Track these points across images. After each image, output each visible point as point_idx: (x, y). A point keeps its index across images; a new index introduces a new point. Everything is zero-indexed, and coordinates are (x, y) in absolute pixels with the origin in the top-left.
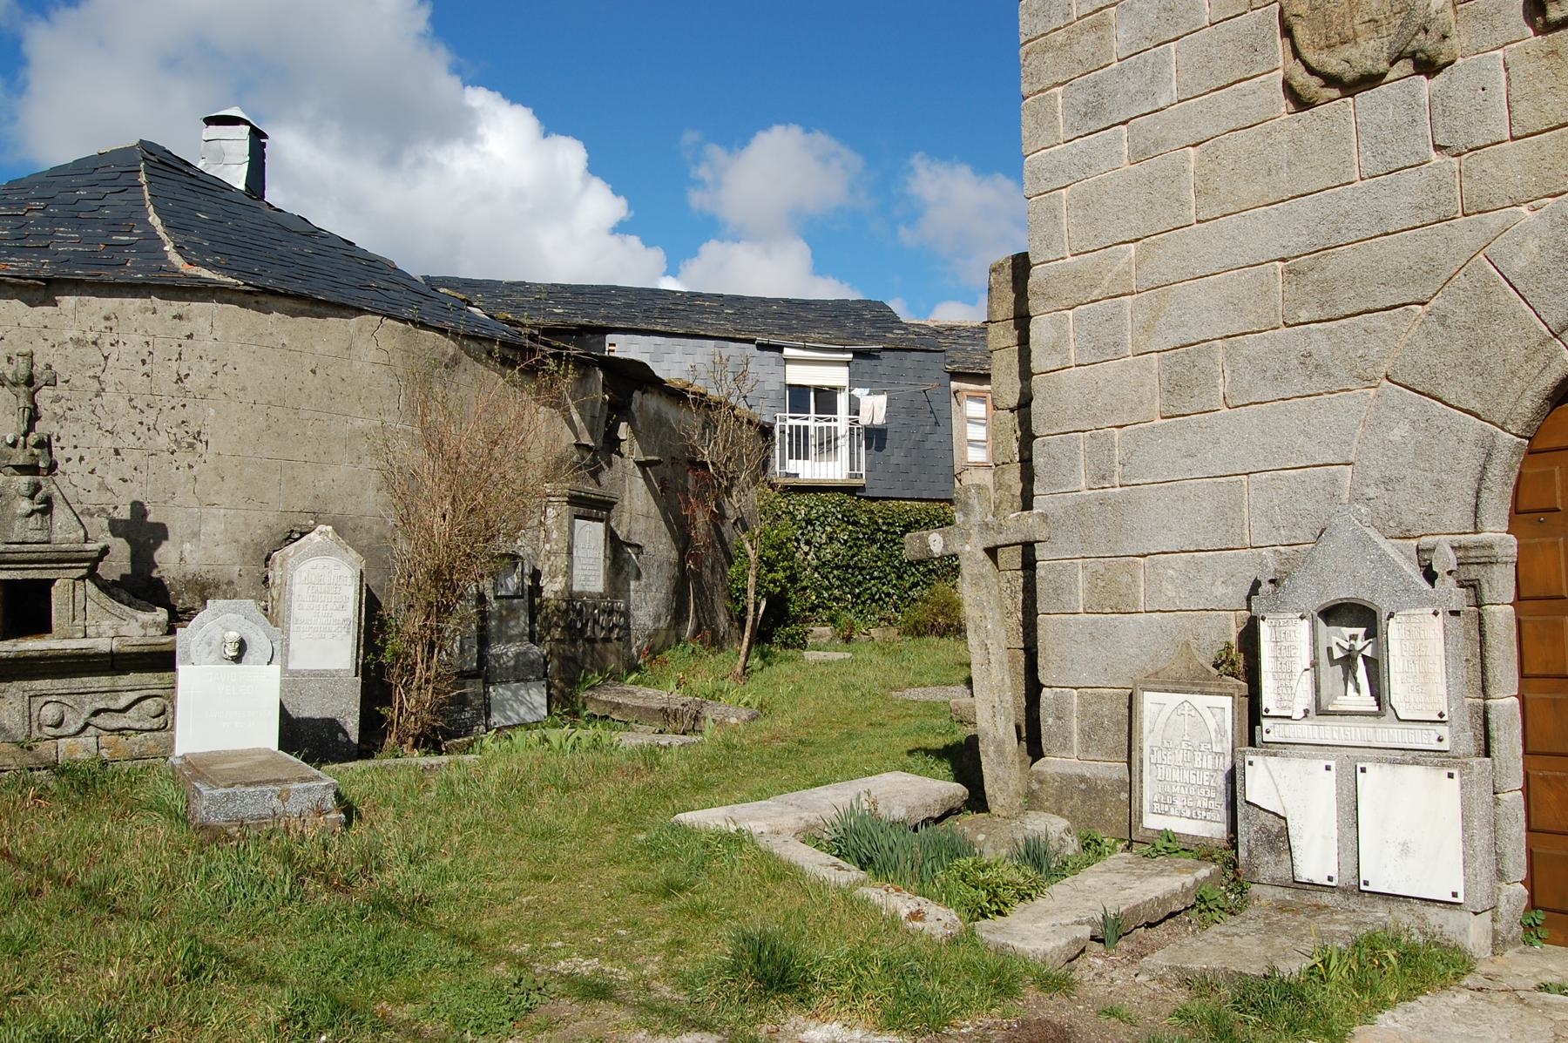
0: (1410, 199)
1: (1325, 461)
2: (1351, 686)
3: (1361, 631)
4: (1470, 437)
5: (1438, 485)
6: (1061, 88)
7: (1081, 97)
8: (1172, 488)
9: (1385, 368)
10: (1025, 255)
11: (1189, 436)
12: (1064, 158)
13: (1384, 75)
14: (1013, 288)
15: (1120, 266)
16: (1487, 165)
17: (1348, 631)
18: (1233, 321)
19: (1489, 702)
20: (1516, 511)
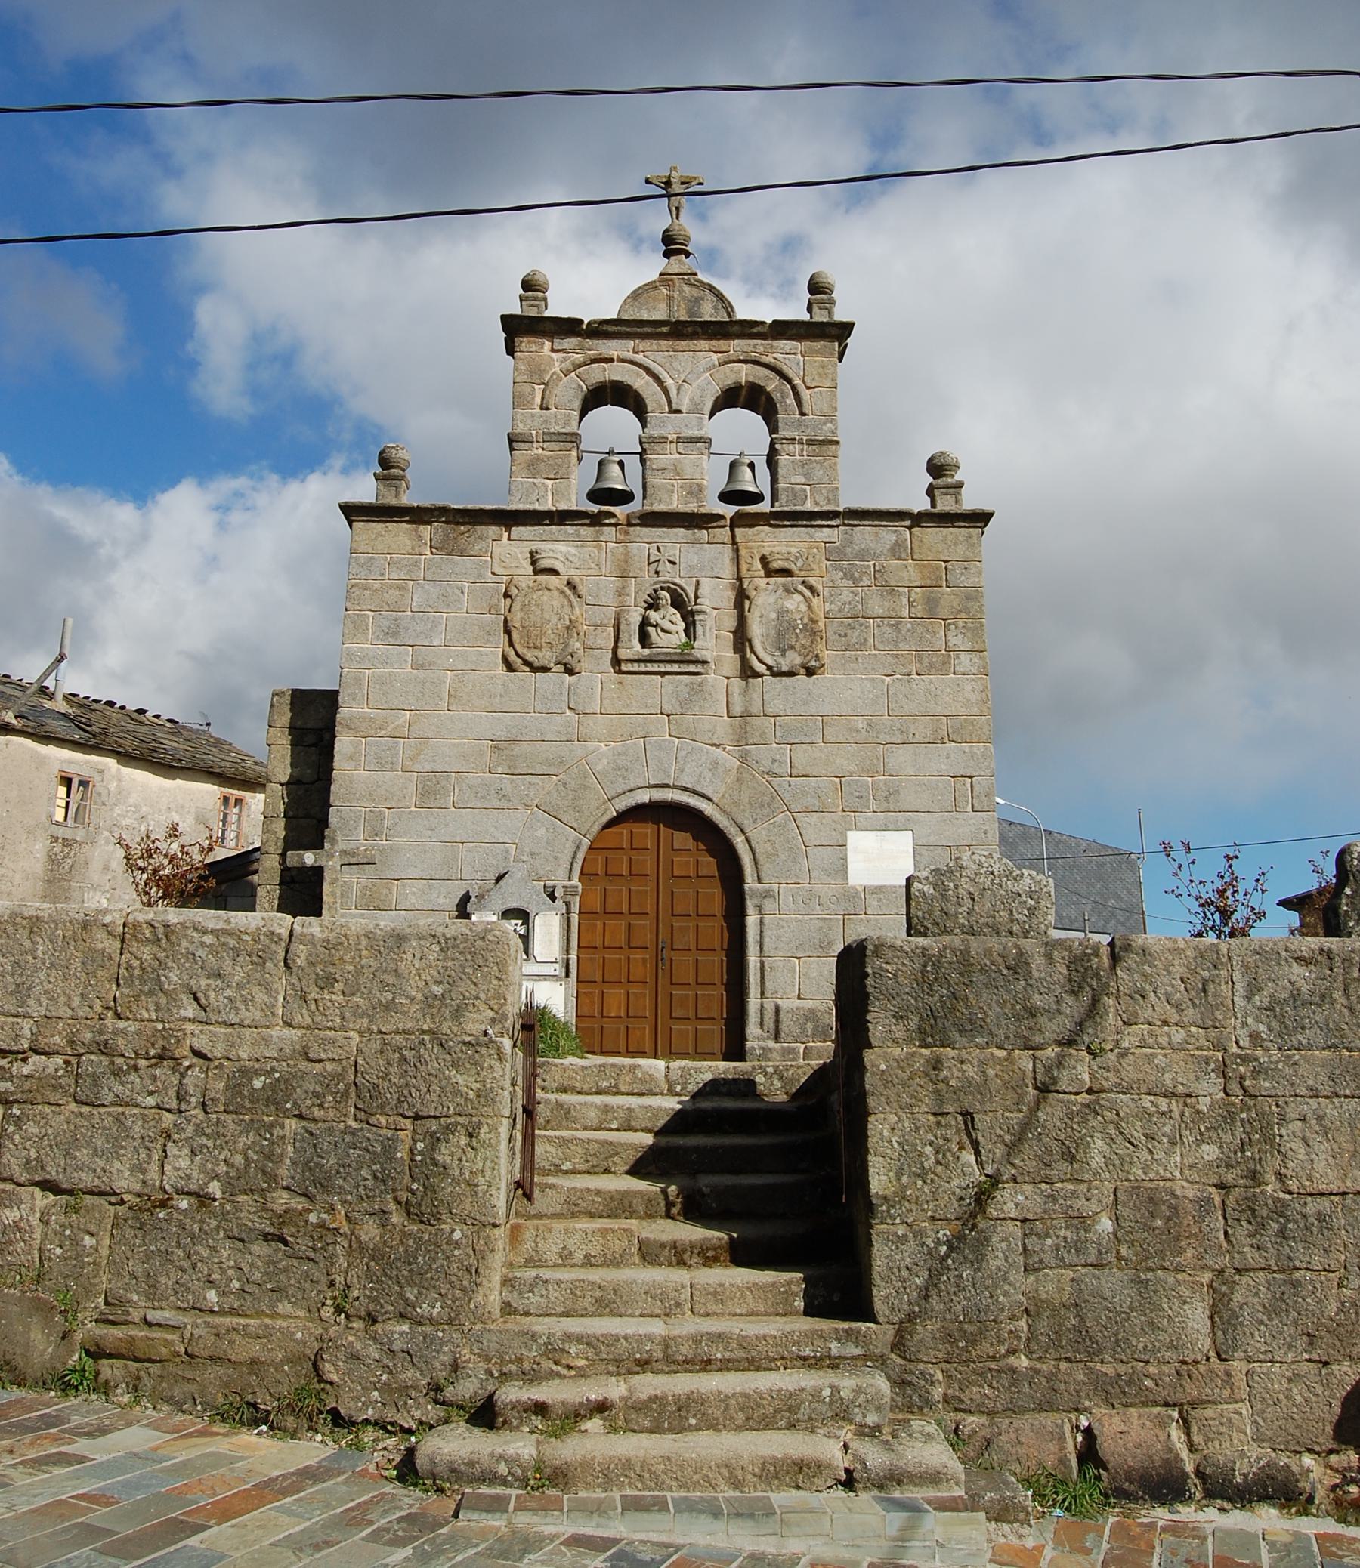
3: (520, 922)
4: (571, 839)
5: (556, 858)
6: (373, 613)
7: (386, 623)
9: (535, 803)
10: (329, 700)
11: (432, 819)
15: (400, 722)
16: (591, 722)
17: (514, 922)
20: (582, 874)
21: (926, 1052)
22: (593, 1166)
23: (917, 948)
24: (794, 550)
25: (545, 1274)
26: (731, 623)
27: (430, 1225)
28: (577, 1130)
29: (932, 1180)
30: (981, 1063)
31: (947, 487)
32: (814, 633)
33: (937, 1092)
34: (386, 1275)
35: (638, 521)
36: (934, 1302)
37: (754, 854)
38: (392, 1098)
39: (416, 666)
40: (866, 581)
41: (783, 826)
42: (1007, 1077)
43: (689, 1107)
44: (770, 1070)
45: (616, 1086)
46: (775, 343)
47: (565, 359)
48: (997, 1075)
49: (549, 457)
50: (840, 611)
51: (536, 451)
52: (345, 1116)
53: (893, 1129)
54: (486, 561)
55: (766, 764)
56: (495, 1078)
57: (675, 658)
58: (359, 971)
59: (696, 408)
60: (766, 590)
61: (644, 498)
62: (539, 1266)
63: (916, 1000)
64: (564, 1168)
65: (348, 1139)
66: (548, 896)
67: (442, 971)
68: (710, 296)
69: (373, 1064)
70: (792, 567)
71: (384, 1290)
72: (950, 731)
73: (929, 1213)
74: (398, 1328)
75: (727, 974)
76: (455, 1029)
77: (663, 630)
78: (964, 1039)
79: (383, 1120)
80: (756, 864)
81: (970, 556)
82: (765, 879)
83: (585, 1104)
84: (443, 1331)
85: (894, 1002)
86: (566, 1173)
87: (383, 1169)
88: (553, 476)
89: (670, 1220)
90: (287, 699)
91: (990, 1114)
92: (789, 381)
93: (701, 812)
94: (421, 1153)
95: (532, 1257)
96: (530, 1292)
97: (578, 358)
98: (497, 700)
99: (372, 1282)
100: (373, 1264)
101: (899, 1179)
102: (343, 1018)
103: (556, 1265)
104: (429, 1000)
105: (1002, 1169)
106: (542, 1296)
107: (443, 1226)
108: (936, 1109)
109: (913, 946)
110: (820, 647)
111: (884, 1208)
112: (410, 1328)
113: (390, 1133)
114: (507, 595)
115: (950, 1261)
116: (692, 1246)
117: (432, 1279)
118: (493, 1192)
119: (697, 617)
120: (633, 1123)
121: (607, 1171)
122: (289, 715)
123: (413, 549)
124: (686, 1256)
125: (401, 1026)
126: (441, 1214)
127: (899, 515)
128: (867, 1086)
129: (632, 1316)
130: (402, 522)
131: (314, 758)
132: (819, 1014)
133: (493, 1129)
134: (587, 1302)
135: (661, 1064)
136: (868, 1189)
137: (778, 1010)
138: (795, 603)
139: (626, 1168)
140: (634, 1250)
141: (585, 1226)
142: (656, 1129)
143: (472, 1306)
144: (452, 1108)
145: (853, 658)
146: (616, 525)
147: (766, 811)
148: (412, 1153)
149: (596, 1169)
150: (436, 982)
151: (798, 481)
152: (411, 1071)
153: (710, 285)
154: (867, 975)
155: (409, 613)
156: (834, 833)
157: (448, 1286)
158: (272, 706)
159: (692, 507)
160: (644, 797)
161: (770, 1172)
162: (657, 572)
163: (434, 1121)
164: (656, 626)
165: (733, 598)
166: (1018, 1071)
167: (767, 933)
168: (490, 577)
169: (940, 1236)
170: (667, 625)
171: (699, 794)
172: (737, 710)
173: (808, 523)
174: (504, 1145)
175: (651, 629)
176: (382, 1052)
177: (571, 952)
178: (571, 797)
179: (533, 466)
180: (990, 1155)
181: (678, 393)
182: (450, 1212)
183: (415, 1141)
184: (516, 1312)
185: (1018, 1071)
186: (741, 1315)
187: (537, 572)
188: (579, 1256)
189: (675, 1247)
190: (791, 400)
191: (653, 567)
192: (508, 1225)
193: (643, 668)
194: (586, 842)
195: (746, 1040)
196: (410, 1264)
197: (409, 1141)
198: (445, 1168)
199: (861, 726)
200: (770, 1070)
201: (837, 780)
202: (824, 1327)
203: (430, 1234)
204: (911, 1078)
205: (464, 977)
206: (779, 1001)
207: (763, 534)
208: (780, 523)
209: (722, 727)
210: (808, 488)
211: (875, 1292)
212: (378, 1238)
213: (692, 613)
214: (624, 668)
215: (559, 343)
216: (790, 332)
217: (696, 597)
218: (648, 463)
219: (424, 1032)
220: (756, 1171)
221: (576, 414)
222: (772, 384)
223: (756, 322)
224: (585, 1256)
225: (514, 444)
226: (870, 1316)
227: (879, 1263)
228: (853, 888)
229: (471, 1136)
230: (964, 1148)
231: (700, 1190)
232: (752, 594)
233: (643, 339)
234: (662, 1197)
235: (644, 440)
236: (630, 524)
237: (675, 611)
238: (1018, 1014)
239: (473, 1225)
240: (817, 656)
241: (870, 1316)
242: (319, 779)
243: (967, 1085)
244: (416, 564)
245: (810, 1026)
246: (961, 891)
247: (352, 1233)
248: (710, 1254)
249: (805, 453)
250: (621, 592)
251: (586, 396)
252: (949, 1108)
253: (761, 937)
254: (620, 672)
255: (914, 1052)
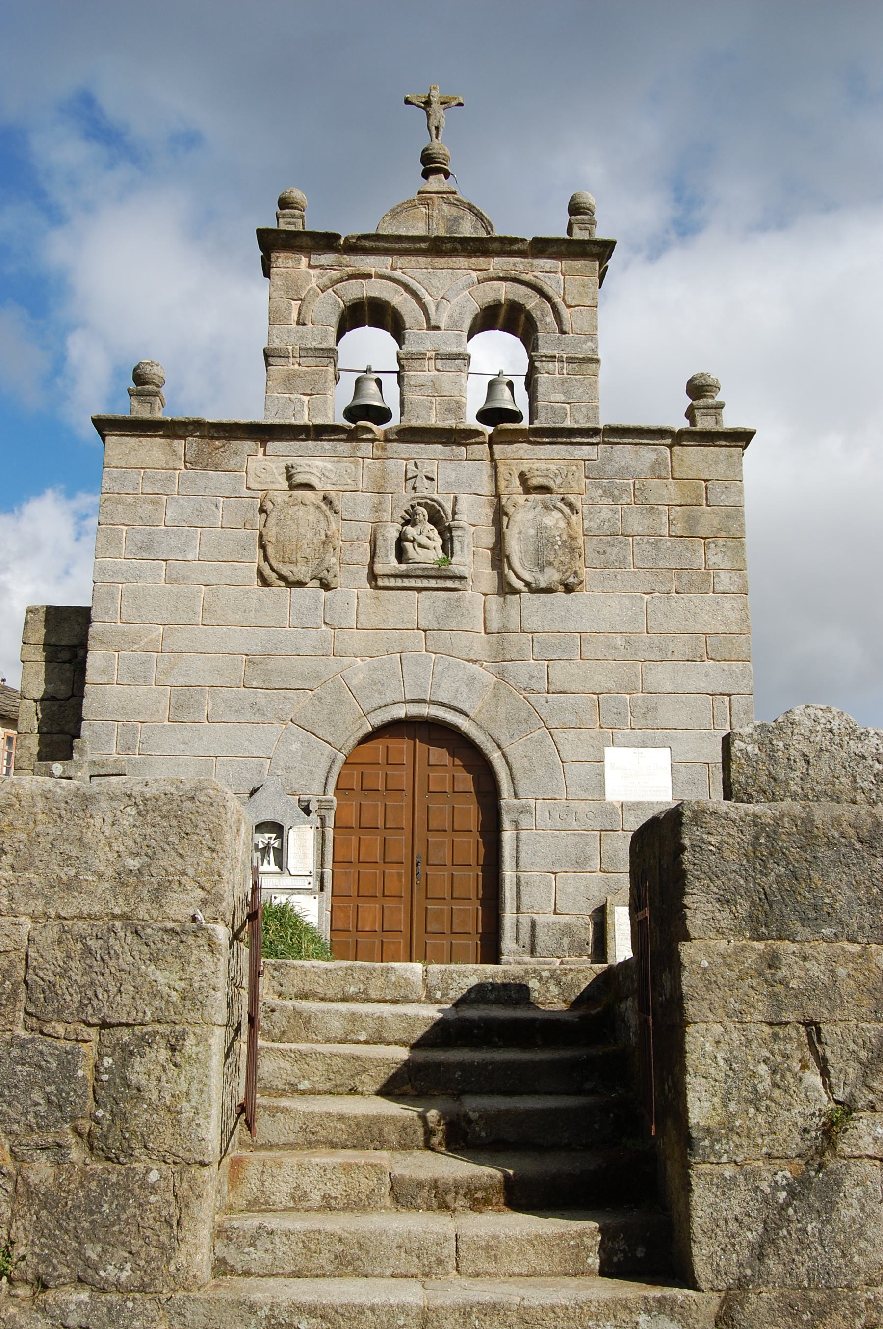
0: (311, 642)
1: (258, 755)
2: (266, 862)
3: (274, 835)
4: (326, 753)
5: (311, 772)
6: (126, 528)
7: (139, 537)
8: (172, 759)
9: (290, 717)
11: (185, 733)
12: (124, 567)
13: (307, 584)
14: (45, 626)
15: (154, 636)
16: (346, 637)
17: (267, 835)
18: (217, 679)
19: (324, 870)
20: (337, 789)
21: (760, 945)
22: (336, 1086)
23: (747, 815)
24: (553, 468)
25: (272, 1222)
26: (489, 539)
27: (119, 1163)
28: (318, 1042)
29: (768, 1107)
30: (829, 960)
31: (708, 408)
32: (573, 550)
33: (773, 996)
34: (61, 1227)
35: (395, 437)
36: (771, 1263)
37: (510, 770)
38: (73, 1000)
39: (170, 580)
40: (626, 499)
41: (540, 742)
42: (862, 978)
43: (452, 1016)
44: (546, 974)
45: (365, 991)
46: (536, 262)
47: (322, 275)
48: (849, 975)
49: (305, 373)
50: (599, 528)
51: (292, 367)
52: (11, 1023)
53: (718, 1042)
54: (241, 476)
55: (524, 680)
56: (205, 975)
57: (433, 573)
58: (34, 839)
59: (455, 325)
60: (525, 506)
61: (402, 414)
62: (265, 1211)
63: (746, 880)
64: (301, 1087)
65: (15, 1052)
66: (303, 809)
67: (139, 840)
68: (469, 216)
69: (48, 957)
70: (551, 484)
71: (57, 1247)
72: (709, 649)
73: (765, 1150)
74: (74, 1297)
75: (483, 890)
76: (155, 913)
77: (420, 546)
78: (807, 930)
79: (60, 1029)
80: (513, 779)
81: (731, 475)
82: (521, 794)
83: (328, 1011)
84: (134, 1300)
85: (719, 882)
86: (303, 1093)
87: (60, 1091)
88: (309, 392)
89: (430, 1152)
90: (42, 616)
91: (842, 1024)
92: (549, 299)
93: (458, 728)
94: (108, 1070)
95: (256, 1199)
96: (251, 1245)
97: (335, 274)
98: (252, 614)
99: (42, 1235)
100: (44, 1213)
101: (725, 1106)
102: (12, 899)
103: (287, 1209)
104: (122, 878)
105: (857, 1093)
106: (267, 1251)
107: (136, 1165)
108: (773, 1017)
109: (742, 813)
110: (579, 564)
111: (707, 1143)
112: (90, 1297)
113: (69, 1045)
114: (262, 510)
115: (791, 1211)
116: (457, 1185)
117: (121, 1232)
118: (201, 1121)
119: (454, 533)
120: (385, 1035)
121: (353, 1091)
122: (44, 631)
123: (167, 463)
124: (449, 1198)
125: (86, 910)
126: (133, 1149)
127: (661, 433)
128: (684, 987)
129: (381, 1276)
130: (156, 436)
131: (68, 674)
132: (575, 929)
133: (202, 1040)
134: (324, 1259)
135: (418, 967)
136: (686, 1120)
137: (533, 925)
138: (554, 520)
139: (377, 1087)
140: (385, 1190)
141: (324, 1160)
142: (412, 1042)
143: (172, 1268)
144: (149, 1013)
145: (612, 575)
146: (373, 441)
147: (523, 726)
148: (98, 1071)
149: (340, 1089)
150: (131, 853)
151: (558, 399)
152: (97, 965)
153: (469, 204)
154: (683, 849)
155: (163, 528)
156: (591, 749)
157: (141, 1242)
158: (26, 623)
159: (449, 423)
160: (400, 712)
161: (550, 1093)
162: (414, 488)
163: (125, 1030)
164: (412, 541)
165: (491, 515)
166: (875, 970)
167: (523, 848)
168: (245, 492)
169: (778, 1178)
170: (424, 540)
171: (456, 709)
172: (495, 626)
173: (568, 440)
174: (216, 1061)
175: (408, 545)
176: (60, 942)
177: (326, 865)
178: (325, 712)
179: (289, 382)
180: (842, 1076)
181: (437, 309)
182: (145, 1147)
183: (101, 1056)
184: (232, 1271)
185: (875, 970)
186: (520, 1275)
187: (293, 487)
188: (315, 1198)
189: (436, 1187)
190: (550, 318)
191: (410, 483)
192: (226, 1161)
193: (399, 583)
194: (341, 757)
195: (502, 954)
196: (92, 1213)
197: (93, 1055)
198: (139, 1090)
199: (619, 643)
200: (546, 974)
201: (595, 697)
202: (630, 1295)
203: (119, 1174)
204: (740, 978)
205: (167, 847)
206: (535, 916)
207: (522, 451)
208: (539, 440)
209: (479, 644)
210: (568, 406)
211: (695, 1251)
212: (51, 1180)
213: (450, 529)
214: (380, 583)
215: (316, 259)
216: (551, 250)
217: (454, 513)
218: (406, 380)
219: (115, 917)
220: (533, 1092)
221: (333, 331)
222: (532, 302)
223: (516, 238)
224: (324, 1197)
225: (270, 359)
226: (688, 1280)
227: (700, 1213)
228: (611, 804)
229: (173, 1049)
230: (808, 1067)
231: (466, 1115)
232: (510, 510)
233: (401, 255)
234: (420, 1123)
235: (402, 356)
236: (387, 440)
237: (432, 527)
238: (875, 899)
239: (175, 1163)
240: (576, 573)
241: (688, 1280)
242: (73, 696)
243: (812, 987)
244: (170, 479)
245: (566, 941)
246: (792, 751)
247: (19, 1173)
248: (479, 1195)
249: (565, 371)
250: (377, 508)
251: (343, 313)
252: (789, 1016)
253: (517, 852)
254: (377, 588)
255: (744, 946)
